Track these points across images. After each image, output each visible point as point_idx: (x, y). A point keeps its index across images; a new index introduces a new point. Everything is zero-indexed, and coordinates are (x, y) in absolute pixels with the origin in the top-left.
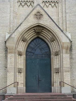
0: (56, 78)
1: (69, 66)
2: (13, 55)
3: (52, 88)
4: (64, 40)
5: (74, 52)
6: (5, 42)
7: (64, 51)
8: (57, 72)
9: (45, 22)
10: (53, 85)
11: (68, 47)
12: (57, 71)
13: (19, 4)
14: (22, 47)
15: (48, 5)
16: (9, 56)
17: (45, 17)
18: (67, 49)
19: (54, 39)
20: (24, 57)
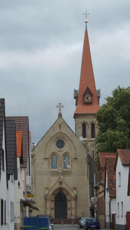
0: (69, 212)
1: (74, 207)
2: (49, 202)
3: (67, 216)
5: (78, 200)
6: (60, 125)
7: (72, 200)
8: (69, 209)
9: (64, 186)
10: (68, 215)
11: (74, 198)
12: (69, 209)
13: (51, 175)
14: (53, 198)
15: (65, 175)
16: (47, 202)
17: (64, 184)
18: (74, 199)
19: (68, 194)
20: (54, 202)
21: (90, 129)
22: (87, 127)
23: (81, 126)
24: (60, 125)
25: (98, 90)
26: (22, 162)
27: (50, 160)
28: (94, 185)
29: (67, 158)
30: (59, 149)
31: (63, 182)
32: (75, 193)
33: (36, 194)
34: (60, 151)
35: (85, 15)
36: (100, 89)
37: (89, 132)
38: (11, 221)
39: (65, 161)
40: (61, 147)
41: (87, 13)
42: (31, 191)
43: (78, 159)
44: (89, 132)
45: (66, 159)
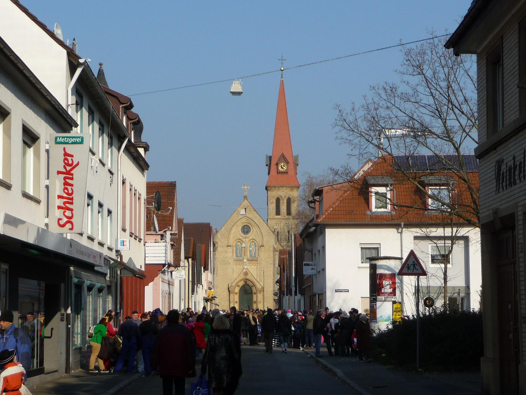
4: (259, 286)
9: (249, 277)
16: (231, 295)
17: (249, 274)
19: (254, 285)
21: (285, 204)
22: (281, 202)
23: (274, 201)
24: (245, 209)
25: (295, 156)
26: (204, 268)
27: (235, 248)
28: (431, 186)
29: (253, 245)
30: (244, 236)
31: (248, 272)
32: (262, 285)
33: (218, 286)
34: (246, 237)
35: (280, 61)
36: (298, 155)
37: (283, 208)
38: (156, 242)
39: (251, 248)
40: (247, 233)
41: (284, 58)
42: (212, 286)
43: (265, 246)
44: (283, 208)
45: (252, 246)
